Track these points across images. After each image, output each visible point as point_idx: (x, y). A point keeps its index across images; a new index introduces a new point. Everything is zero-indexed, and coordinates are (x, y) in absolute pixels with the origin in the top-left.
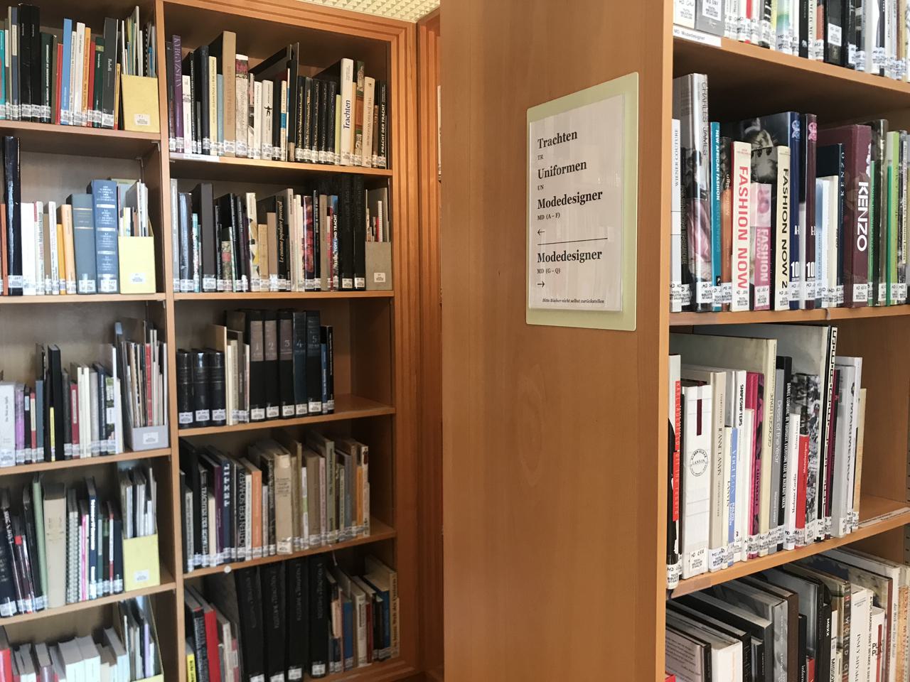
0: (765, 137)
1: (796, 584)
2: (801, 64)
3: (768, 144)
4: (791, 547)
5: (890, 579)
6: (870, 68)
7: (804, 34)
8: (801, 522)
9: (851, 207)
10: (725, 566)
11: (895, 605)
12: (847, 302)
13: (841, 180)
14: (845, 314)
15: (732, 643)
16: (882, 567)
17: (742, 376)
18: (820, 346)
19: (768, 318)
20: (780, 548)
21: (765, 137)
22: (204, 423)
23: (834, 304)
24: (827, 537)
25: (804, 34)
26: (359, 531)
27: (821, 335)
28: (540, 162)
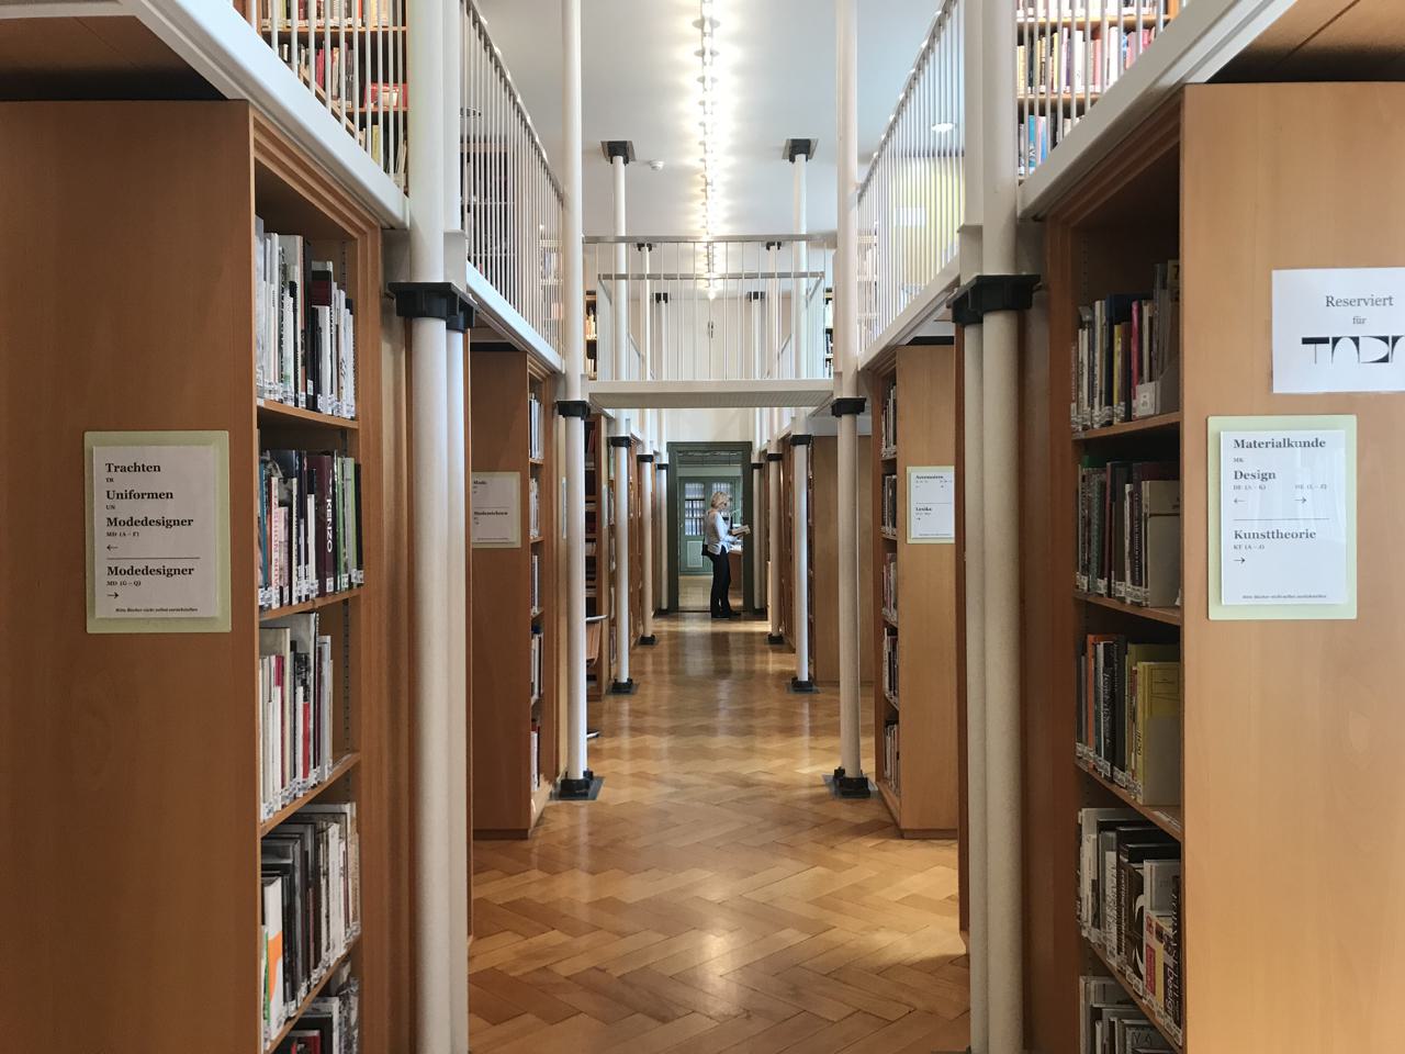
0: (274, 466)
1: (298, 828)
2: (311, 415)
3: (774, 662)
4: (300, 795)
5: (345, 814)
6: (326, 410)
7: (296, 391)
8: (306, 775)
9: (322, 518)
10: (271, 815)
11: (1146, 498)
12: (322, 592)
13: (316, 498)
14: (320, 603)
15: (274, 881)
16: (337, 806)
17: (273, 658)
18: (309, 629)
19: (287, 611)
20: (295, 797)
21: (274, 466)
22: (594, 684)
23: (314, 595)
24: (319, 783)
25: (296, 391)
26: (327, 772)
27: (309, 622)
28: (110, 484)
